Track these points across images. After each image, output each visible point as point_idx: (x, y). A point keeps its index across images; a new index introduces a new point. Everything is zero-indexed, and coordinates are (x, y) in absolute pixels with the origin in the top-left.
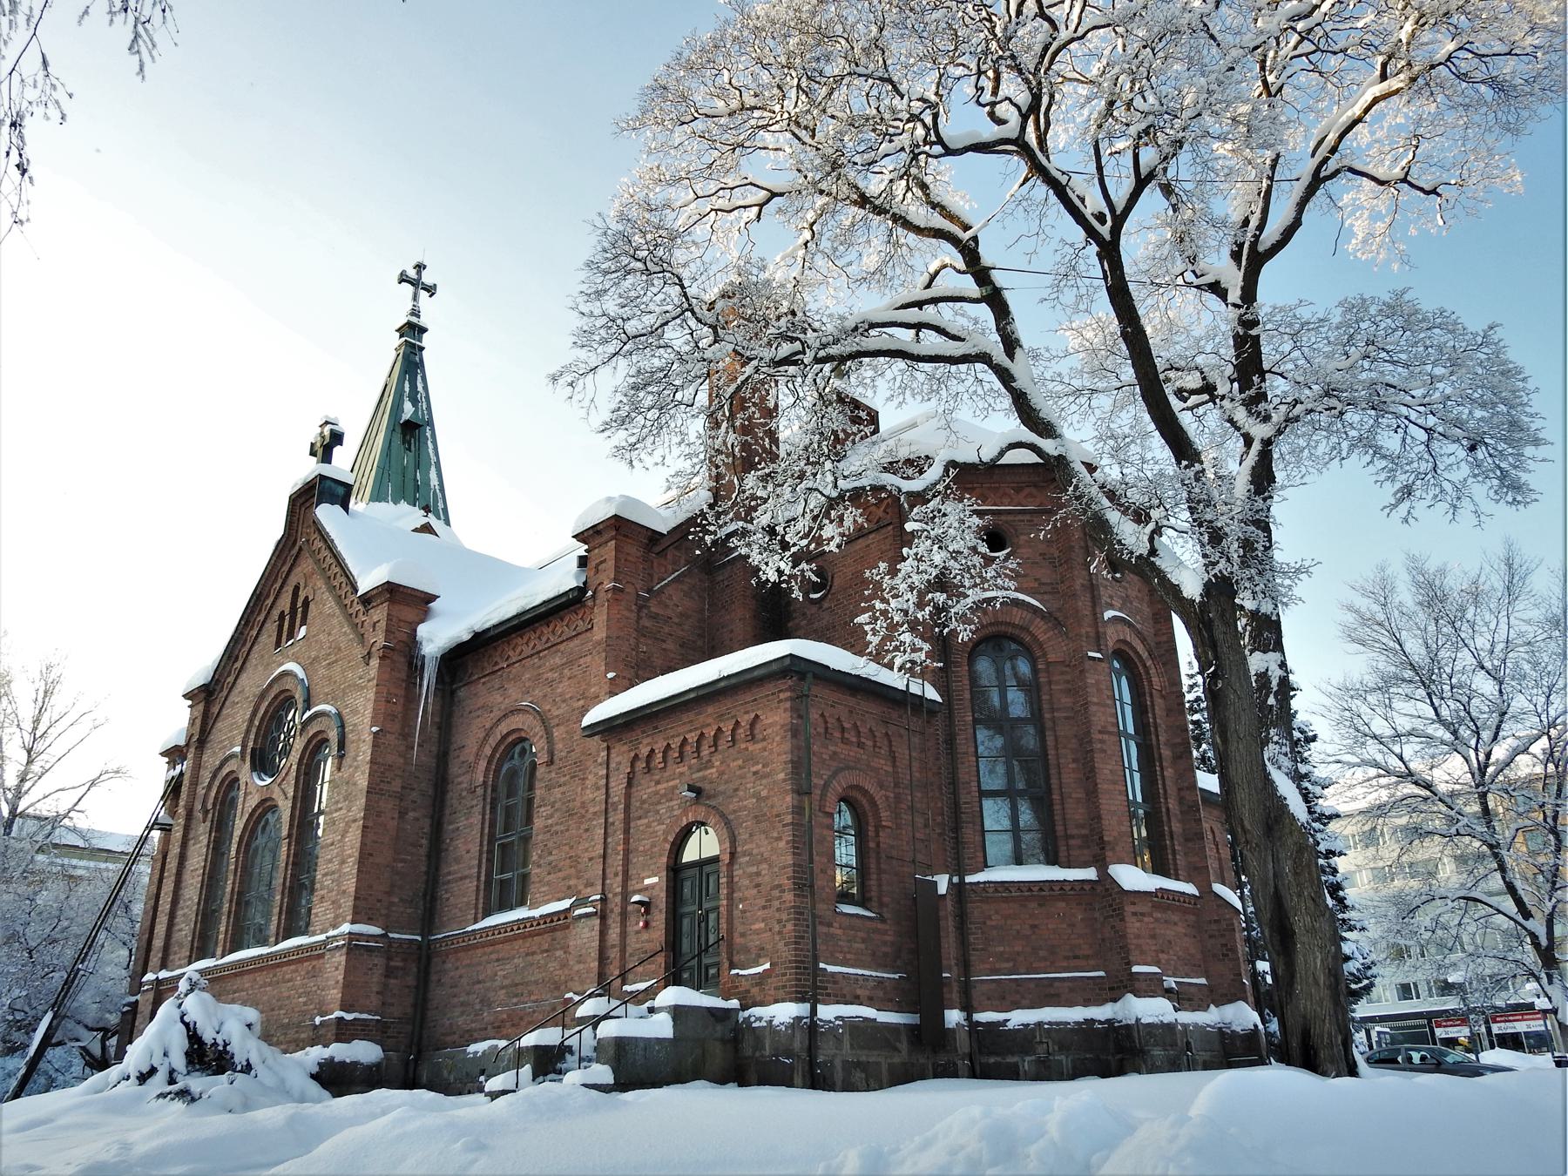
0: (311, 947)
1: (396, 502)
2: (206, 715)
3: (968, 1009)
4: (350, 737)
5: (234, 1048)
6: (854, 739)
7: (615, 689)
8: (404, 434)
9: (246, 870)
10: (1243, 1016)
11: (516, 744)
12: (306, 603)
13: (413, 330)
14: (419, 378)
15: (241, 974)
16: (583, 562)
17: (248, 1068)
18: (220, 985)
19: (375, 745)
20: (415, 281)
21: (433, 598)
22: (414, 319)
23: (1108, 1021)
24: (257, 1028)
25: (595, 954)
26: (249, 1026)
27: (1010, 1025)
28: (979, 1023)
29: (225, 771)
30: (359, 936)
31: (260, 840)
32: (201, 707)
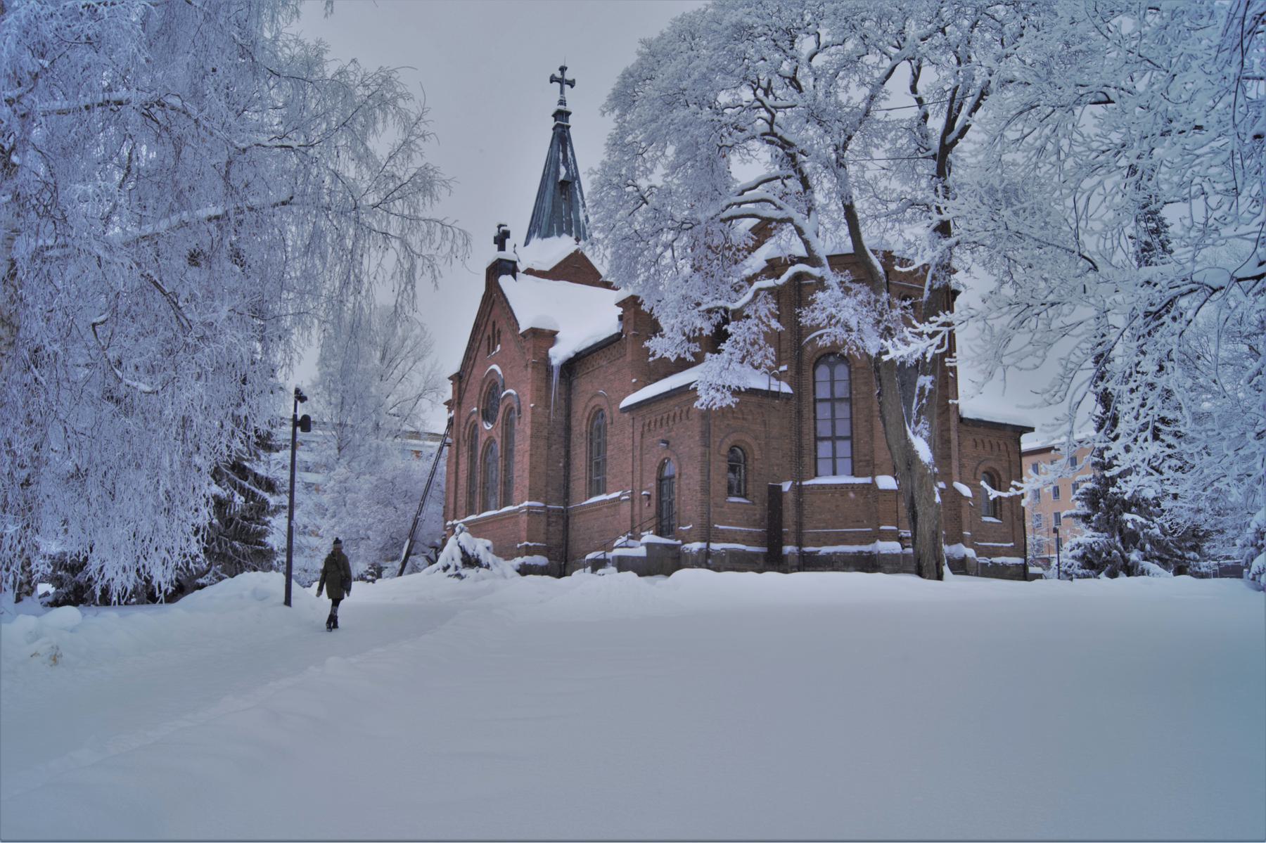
0: (514, 512)
1: (559, 235)
2: (460, 388)
3: (799, 544)
4: (523, 408)
5: (481, 557)
6: (740, 416)
7: (636, 388)
8: (561, 189)
9: (486, 472)
10: (893, 547)
11: (598, 413)
12: (499, 332)
13: (561, 115)
14: (569, 149)
15: (488, 523)
16: (621, 318)
17: (488, 566)
18: (476, 529)
19: (533, 414)
20: (562, 80)
21: (557, 332)
22: (562, 107)
23: (870, 552)
24: (492, 549)
25: (629, 518)
26: (488, 548)
27: (820, 553)
28: (804, 552)
29: (471, 420)
30: (532, 507)
31: (490, 457)
32: (457, 385)
